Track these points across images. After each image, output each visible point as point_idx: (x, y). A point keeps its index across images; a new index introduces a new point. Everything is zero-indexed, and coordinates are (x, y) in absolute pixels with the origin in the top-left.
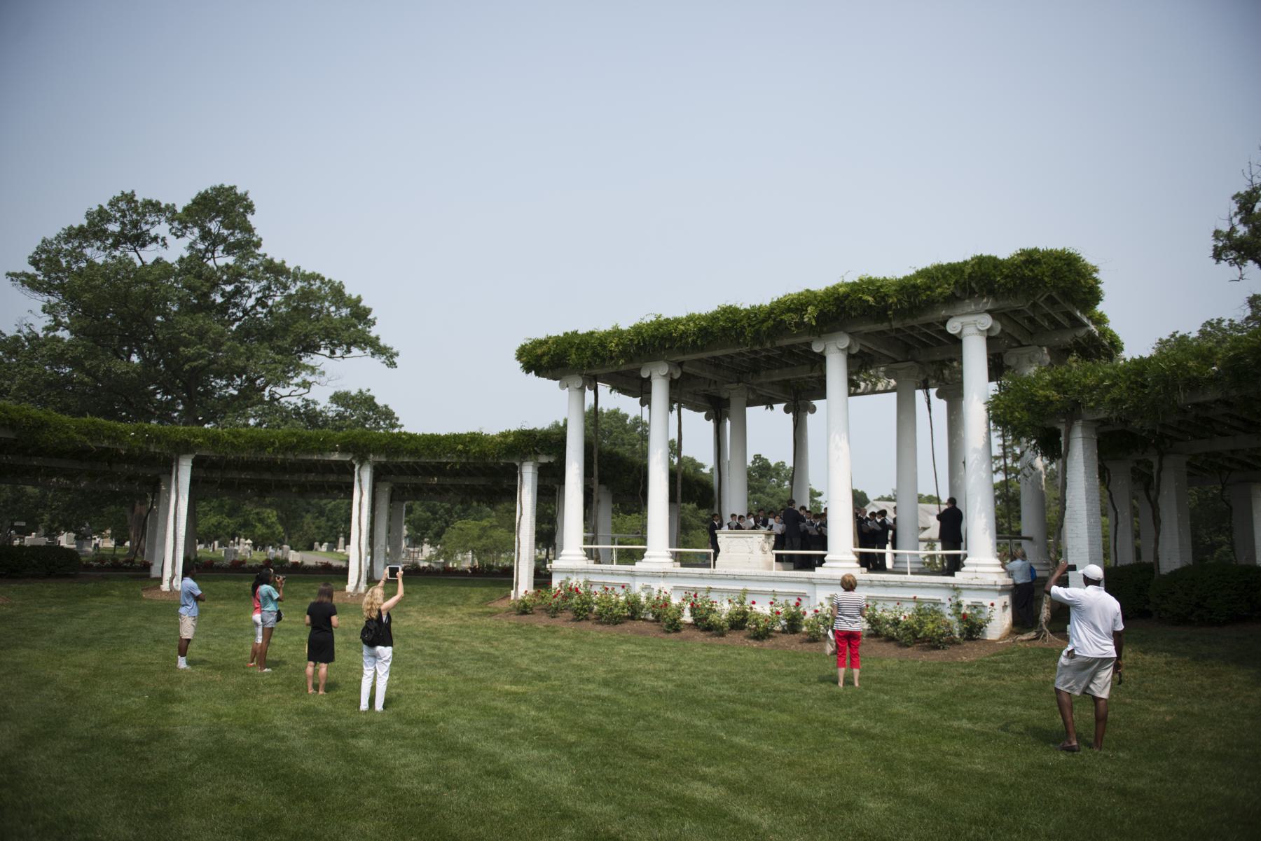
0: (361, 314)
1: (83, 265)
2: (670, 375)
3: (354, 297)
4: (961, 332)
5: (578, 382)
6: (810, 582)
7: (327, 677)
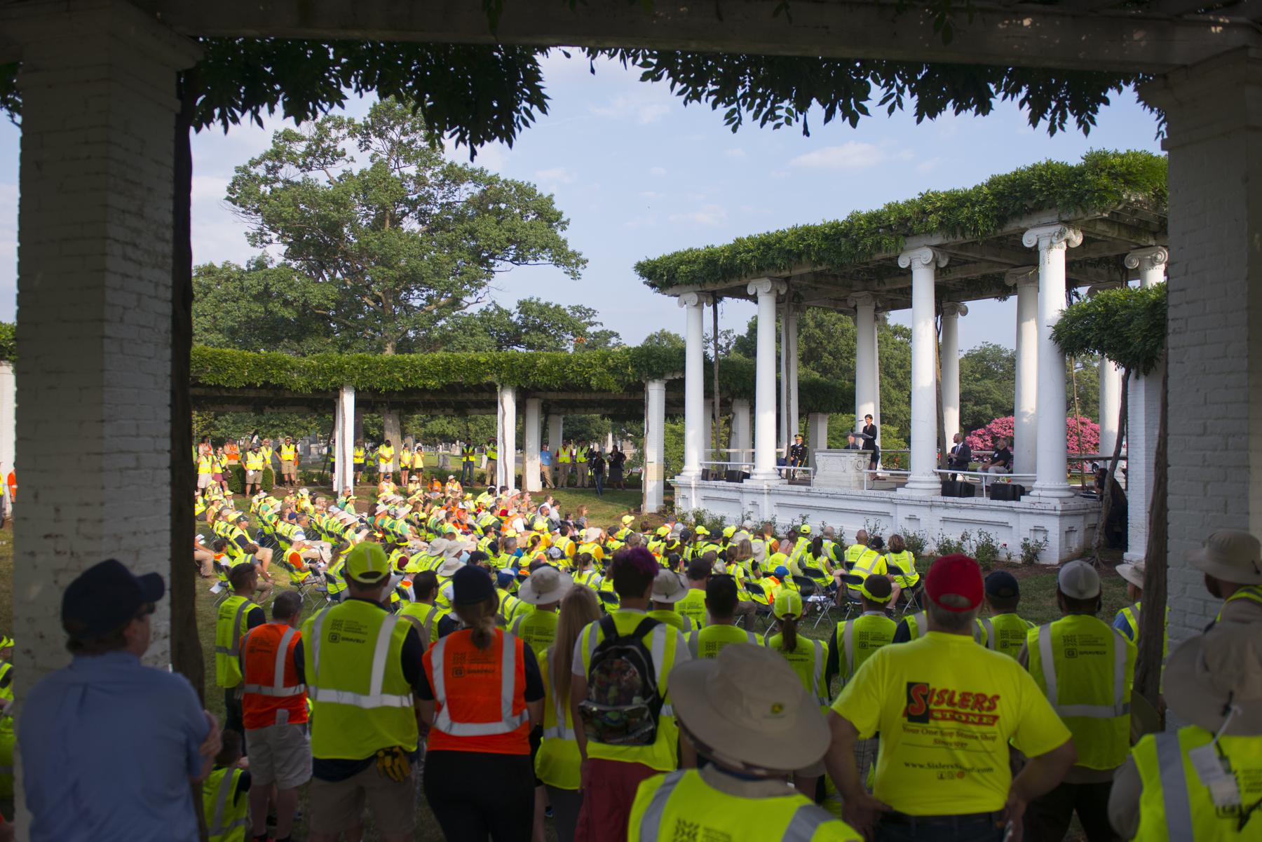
0: (548, 216)
1: (279, 185)
2: (936, 261)
3: (546, 195)
4: (1036, 246)
5: (693, 298)
6: (741, 491)
7: (528, 602)
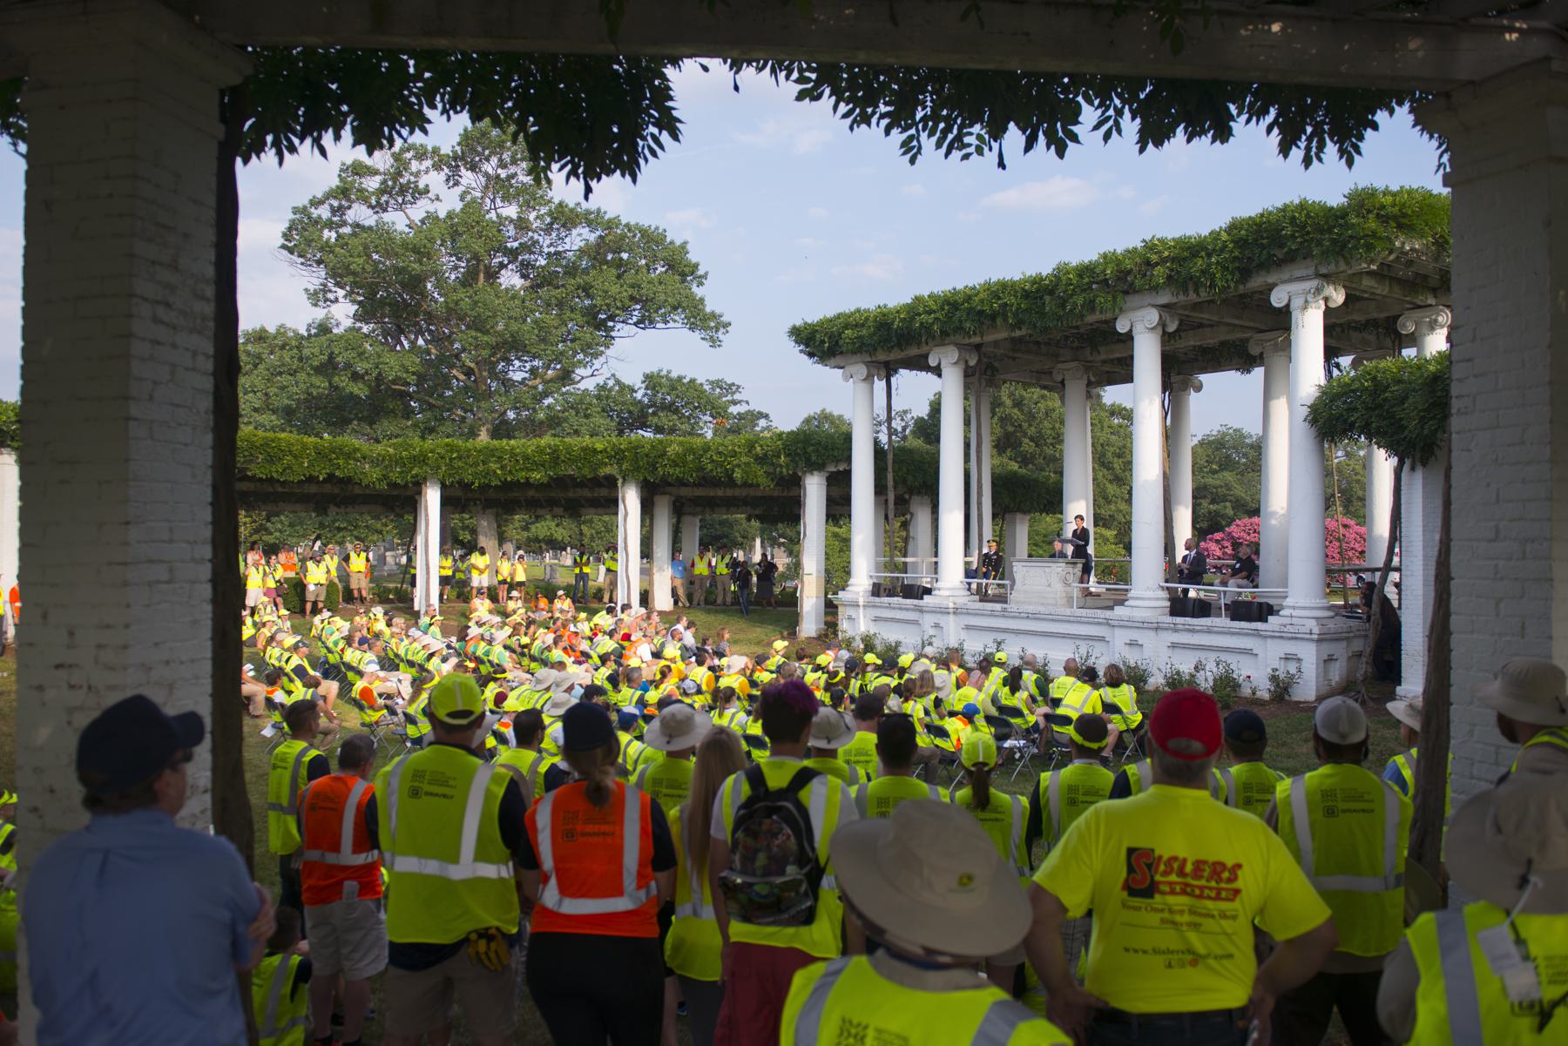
0: (681, 268)
1: (347, 230)
2: (1162, 324)
3: (678, 243)
4: (1288, 306)
5: (861, 370)
